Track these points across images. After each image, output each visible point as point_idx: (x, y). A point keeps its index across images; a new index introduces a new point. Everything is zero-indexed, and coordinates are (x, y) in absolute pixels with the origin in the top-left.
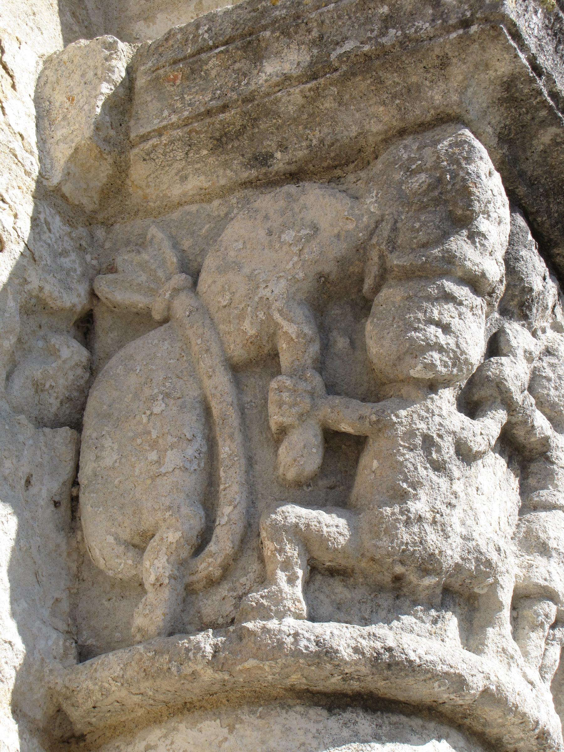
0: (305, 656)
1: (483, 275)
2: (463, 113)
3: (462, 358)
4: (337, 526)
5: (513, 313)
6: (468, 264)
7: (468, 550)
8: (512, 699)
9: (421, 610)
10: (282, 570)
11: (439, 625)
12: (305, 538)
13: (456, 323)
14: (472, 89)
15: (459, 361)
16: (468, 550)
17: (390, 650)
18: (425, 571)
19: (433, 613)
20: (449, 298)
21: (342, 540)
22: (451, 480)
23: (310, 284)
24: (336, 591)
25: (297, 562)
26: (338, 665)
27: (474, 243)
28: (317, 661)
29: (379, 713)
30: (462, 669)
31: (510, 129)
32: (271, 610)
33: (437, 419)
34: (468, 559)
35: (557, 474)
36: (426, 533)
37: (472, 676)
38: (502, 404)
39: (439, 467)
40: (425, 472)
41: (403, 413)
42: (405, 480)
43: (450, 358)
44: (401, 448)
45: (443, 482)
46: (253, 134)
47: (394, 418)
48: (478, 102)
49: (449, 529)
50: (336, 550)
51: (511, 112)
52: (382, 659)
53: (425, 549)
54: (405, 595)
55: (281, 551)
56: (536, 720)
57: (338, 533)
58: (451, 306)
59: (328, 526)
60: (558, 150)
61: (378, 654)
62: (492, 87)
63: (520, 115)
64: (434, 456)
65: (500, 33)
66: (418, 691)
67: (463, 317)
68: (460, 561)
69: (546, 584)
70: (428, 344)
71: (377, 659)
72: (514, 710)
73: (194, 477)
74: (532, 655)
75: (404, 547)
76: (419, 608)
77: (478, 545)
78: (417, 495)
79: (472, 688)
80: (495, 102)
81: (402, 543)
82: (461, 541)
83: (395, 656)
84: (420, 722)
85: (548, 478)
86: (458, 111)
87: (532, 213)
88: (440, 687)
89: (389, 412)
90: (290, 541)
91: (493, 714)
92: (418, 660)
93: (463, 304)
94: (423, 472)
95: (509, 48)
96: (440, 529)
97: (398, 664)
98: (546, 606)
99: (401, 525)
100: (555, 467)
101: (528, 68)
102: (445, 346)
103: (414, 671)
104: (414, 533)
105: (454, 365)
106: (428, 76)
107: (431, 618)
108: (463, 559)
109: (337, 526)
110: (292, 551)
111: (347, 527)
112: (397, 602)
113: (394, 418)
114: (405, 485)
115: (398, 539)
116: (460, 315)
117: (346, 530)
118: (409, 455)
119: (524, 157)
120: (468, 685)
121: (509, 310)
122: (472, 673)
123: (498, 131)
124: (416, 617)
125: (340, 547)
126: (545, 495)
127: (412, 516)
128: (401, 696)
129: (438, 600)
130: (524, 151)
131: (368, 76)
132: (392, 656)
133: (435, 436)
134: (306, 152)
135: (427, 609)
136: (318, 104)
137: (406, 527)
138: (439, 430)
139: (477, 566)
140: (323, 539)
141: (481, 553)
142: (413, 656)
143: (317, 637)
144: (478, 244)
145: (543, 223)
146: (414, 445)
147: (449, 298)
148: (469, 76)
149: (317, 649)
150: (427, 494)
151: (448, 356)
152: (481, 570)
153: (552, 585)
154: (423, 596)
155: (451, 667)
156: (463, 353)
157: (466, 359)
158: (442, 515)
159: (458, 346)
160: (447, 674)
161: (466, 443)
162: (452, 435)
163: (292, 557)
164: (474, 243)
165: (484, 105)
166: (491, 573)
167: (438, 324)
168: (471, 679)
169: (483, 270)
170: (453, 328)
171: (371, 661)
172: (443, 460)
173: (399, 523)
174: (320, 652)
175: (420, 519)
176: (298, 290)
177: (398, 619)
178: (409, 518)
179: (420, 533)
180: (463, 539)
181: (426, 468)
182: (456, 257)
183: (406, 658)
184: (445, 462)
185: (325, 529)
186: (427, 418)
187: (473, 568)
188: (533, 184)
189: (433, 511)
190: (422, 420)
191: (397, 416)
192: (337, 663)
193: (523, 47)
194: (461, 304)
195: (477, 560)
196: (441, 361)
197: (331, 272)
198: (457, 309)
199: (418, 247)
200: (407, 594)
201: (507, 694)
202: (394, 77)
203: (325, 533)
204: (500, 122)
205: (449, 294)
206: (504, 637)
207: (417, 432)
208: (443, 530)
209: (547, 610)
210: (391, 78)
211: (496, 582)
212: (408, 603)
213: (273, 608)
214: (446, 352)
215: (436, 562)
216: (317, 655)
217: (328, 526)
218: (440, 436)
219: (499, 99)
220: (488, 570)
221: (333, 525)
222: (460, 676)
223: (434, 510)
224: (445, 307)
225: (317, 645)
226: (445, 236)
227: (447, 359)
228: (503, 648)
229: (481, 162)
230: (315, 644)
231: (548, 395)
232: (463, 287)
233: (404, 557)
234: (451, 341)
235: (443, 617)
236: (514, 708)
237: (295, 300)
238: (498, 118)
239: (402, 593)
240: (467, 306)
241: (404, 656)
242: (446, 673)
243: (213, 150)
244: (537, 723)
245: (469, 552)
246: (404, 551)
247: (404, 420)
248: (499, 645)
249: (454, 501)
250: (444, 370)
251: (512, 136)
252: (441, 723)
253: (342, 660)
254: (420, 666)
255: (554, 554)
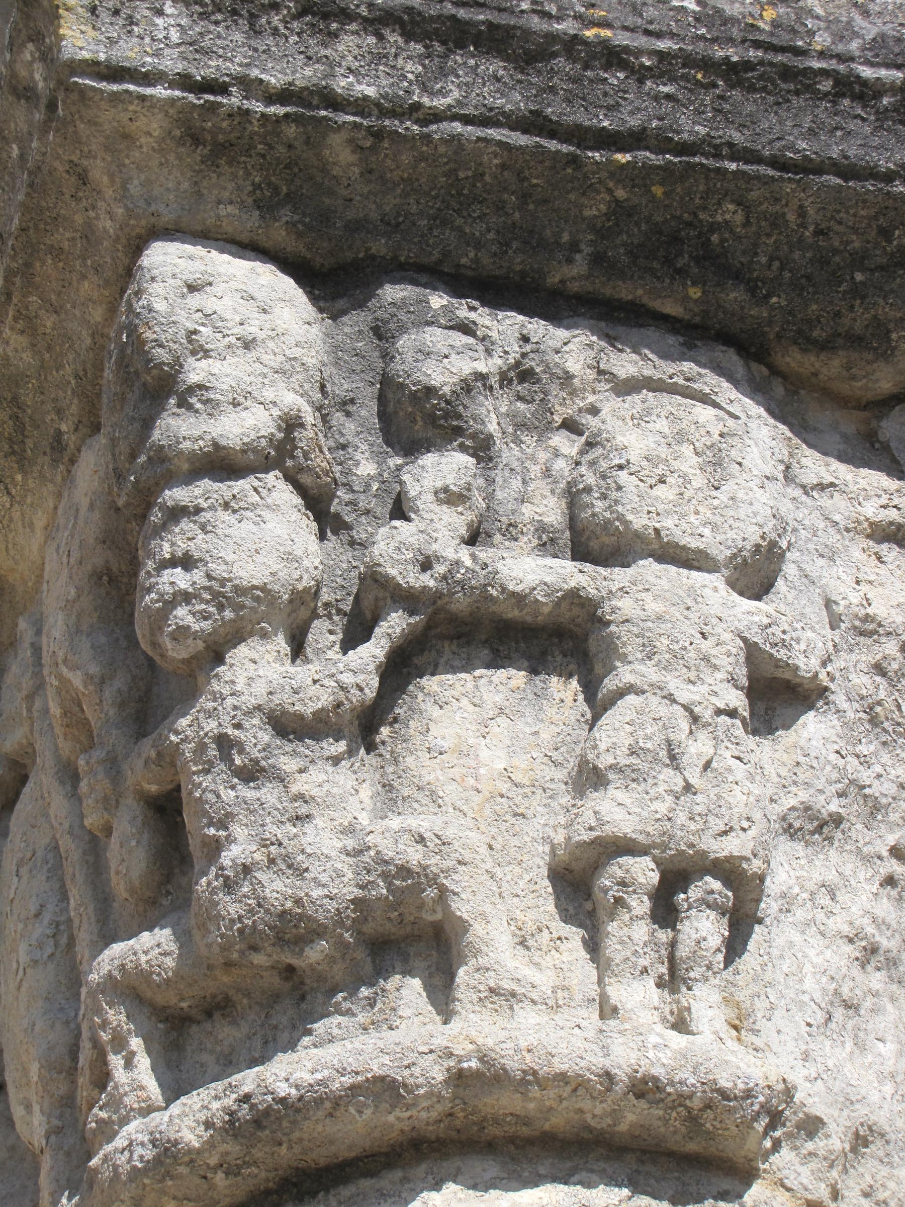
0: (145, 1171)
1: (216, 445)
2: (153, 220)
3: (227, 589)
4: (158, 945)
5: (428, 440)
6: (186, 445)
7: (365, 868)
8: (513, 1065)
9: (345, 999)
10: (115, 1053)
11: (379, 1005)
12: (131, 988)
13: (199, 545)
14: (136, 182)
15: (224, 597)
16: (365, 868)
17: (246, 1098)
18: (301, 942)
19: (364, 992)
20: (177, 513)
21: (170, 962)
22: (283, 781)
23: (91, 597)
24: (220, 1037)
25: (128, 1030)
26: (192, 1161)
27: (190, 407)
28: (163, 1170)
29: (321, 1195)
30: (378, 1066)
31: (269, 184)
32: (113, 1122)
33: (230, 701)
34: (369, 882)
35: (618, 638)
36: (263, 886)
37: (408, 1067)
38: (394, 602)
39: (251, 774)
40: (232, 793)
41: (183, 722)
42: (210, 824)
43: (207, 602)
44: (195, 777)
45: (269, 794)
46: (30, 418)
47: (173, 738)
48: (168, 189)
49: (300, 857)
50: (168, 981)
51: (245, 162)
52: (239, 1119)
53: (267, 911)
54: (312, 989)
55: (105, 1024)
56: (601, 1072)
57: (161, 954)
58: (185, 524)
59: (146, 953)
60: (386, 155)
61: (231, 1114)
62: (172, 157)
63: (263, 156)
64: (238, 762)
65: (82, 91)
66: (359, 1128)
67: (209, 528)
68: (359, 893)
69: (595, 834)
70: (166, 602)
71: (231, 1122)
72: (531, 1079)
73: (51, 966)
74: (617, 961)
75: (239, 925)
76: (340, 996)
77: (378, 852)
78: (230, 835)
79: (418, 1086)
80: (201, 171)
81: (232, 921)
82: (350, 860)
83: (256, 1104)
84: (398, 1174)
85: (612, 653)
86: (143, 222)
87: (440, 262)
88: (360, 1112)
89: (166, 732)
90: (111, 1004)
91: (505, 1102)
92: (293, 1091)
93: (203, 510)
94: (229, 795)
95: (115, 97)
96: (283, 867)
97: (268, 1112)
98: (615, 868)
99: (221, 895)
100: (613, 628)
101: (184, 98)
102: (191, 590)
103: (298, 1111)
104: (244, 896)
105: (221, 608)
106: (84, 203)
107: (365, 1002)
108: (362, 887)
109: (158, 945)
110: (116, 1016)
111: (172, 937)
112: (304, 1006)
113: (173, 738)
114: (212, 831)
115: (223, 919)
116: (203, 528)
117: (172, 944)
118: (206, 781)
119: (339, 202)
120: (405, 1085)
121: (420, 440)
122: (405, 1063)
123: (250, 200)
124: (342, 1014)
125: (170, 974)
126: (610, 684)
127: (229, 873)
128: (320, 1156)
129: (368, 967)
130: (331, 193)
131: (41, 254)
132: (253, 1107)
133: (230, 731)
134: (76, 401)
135: (353, 993)
136: (41, 330)
137: (229, 893)
138: (234, 717)
139: (389, 886)
140: (144, 975)
141: (386, 862)
142: (283, 1089)
143: (151, 1133)
144: (198, 406)
145: (476, 260)
146: (209, 760)
147: (177, 513)
148: (114, 167)
149: (155, 1151)
150: (246, 825)
151: (203, 601)
152: (398, 887)
153: (608, 830)
154: (338, 972)
155: (357, 1073)
156: (223, 582)
157: (236, 587)
158: (280, 844)
159: (209, 577)
160: (354, 1089)
161: (284, 712)
162: (257, 713)
163: (118, 1026)
164: (190, 407)
165: (185, 185)
166: (419, 883)
167: (173, 562)
168: (407, 1073)
169: (213, 439)
170: (196, 555)
171: (226, 1131)
172: (251, 760)
173: (216, 893)
174: (158, 1155)
175: (246, 870)
176: (79, 616)
177: (309, 1032)
178: (227, 878)
179: (255, 890)
180: (354, 856)
181: (233, 787)
182: (163, 447)
183: (273, 1099)
184: (256, 762)
185: (144, 958)
186: (215, 709)
187: (384, 891)
188: (398, 224)
189: (265, 846)
190: (210, 717)
191: (177, 733)
192: (186, 1159)
193: (148, 79)
194: (198, 510)
195: (385, 875)
196: (194, 614)
197: (107, 561)
198: (195, 522)
199: (130, 463)
200: (315, 985)
201: (503, 1061)
202: (62, 235)
203: (144, 966)
204: (239, 188)
205: (173, 508)
206: (488, 969)
207: (206, 740)
208: (290, 866)
209: (620, 873)
210: (62, 237)
211: (443, 891)
212: (320, 998)
213: (115, 1117)
214: (195, 596)
215: (300, 920)
216: (157, 1161)
217: (146, 953)
218: (238, 726)
219: (202, 162)
220: (409, 882)
221: (152, 948)
222: (382, 1079)
223: (264, 844)
224: (177, 530)
225: (154, 1146)
226: (148, 424)
227: (204, 606)
228: (490, 989)
229: (155, 285)
230: (150, 1147)
231: (594, 515)
232: (197, 483)
233: (250, 940)
234: (198, 576)
235: (383, 991)
236: (530, 1078)
237: (82, 631)
238: (231, 186)
239: (306, 988)
240: (212, 508)
241: (269, 1098)
242: (352, 1087)
243: (22, 469)
244: (608, 1075)
245: (368, 872)
246: (241, 931)
247: (188, 733)
248: (481, 988)
249: (303, 810)
250: (206, 625)
251: (285, 189)
252: (445, 1156)
253: (190, 1151)
254: (301, 1098)
255: (611, 776)
